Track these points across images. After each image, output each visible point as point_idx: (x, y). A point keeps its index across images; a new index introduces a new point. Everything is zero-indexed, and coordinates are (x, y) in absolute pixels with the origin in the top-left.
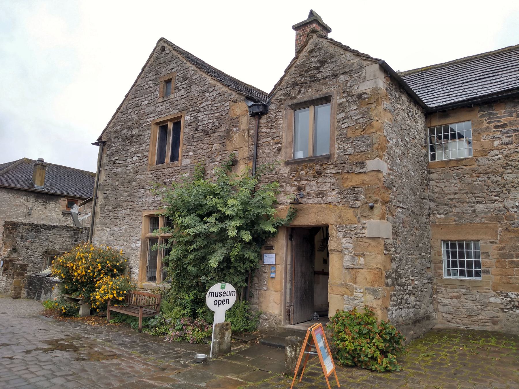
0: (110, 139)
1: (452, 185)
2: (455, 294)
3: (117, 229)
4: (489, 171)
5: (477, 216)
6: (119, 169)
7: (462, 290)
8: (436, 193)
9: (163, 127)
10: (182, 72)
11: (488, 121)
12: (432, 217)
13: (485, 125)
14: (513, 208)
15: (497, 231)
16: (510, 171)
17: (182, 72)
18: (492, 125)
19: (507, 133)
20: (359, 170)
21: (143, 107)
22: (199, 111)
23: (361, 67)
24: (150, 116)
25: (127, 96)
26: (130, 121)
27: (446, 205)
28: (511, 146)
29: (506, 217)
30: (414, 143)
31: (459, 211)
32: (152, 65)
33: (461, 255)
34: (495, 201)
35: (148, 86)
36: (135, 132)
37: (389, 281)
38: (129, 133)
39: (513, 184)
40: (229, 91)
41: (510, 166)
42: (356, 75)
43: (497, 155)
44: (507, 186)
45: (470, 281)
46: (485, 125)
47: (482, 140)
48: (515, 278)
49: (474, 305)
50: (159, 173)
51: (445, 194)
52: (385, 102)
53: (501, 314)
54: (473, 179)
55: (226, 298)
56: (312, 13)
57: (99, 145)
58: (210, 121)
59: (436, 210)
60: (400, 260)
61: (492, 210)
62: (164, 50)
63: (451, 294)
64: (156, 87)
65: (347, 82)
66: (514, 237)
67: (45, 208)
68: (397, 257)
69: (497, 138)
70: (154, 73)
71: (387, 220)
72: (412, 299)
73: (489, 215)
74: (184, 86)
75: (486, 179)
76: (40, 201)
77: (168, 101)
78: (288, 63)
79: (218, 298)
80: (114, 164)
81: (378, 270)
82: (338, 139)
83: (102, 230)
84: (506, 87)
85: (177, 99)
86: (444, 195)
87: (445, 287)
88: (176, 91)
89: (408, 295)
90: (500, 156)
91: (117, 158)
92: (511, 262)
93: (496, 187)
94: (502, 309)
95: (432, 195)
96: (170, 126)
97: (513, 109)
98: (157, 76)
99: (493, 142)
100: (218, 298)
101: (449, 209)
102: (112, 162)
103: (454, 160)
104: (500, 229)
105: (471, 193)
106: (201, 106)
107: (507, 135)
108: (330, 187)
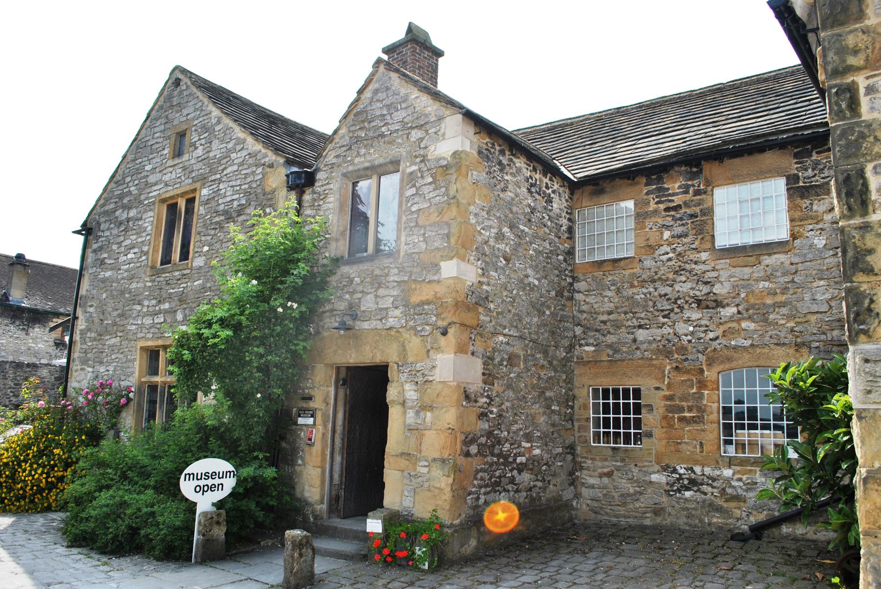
0: (99, 224)
1: (606, 299)
2: (606, 470)
3: (102, 369)
4: (656, 277)
5: (637, 349)
6: (108, 274)
7: (614, 463)
8: (584, 312)
9: (173, 208)
10: (201, 119)
11: (656, 200)
12: (577, 351)
13: (652, 206)
14: (686, 335)
15: (664, 371)
16: (683, 278)
17: (201, 119)
18: (662, 206)
19: (681, 219)
20: (430, 277)
21: (146, 173)
22: (220, 181)
23: (440, 119)
24: (155, 188)
25: (124, 157)
26: (127, 196)
27: (597, 330)
28: (685, 240)
29: (677, 349)
30: (541, 233)
31: (615, 340)
32: (161, 107)
33: (606, 410)
34: (664, 324)
35: (154, 142)
36: (133, 213)
37: (474, 449)
38: (125, 216)
39: (687, 299)
40: (263, 151)
41: (683, 270)
42: (434, 130)
43: (668, 253)
44: (679, 302)
45: (626, 450)
46: (652, 206)
47: (647, 230)
48: (685, 443)
49: (630, 485)
50: (162, 279)
51: (595, 313)
52: (475, 173)
53: (665, 499)
54: (635, 290)
55: (217, 481)
56: (411, 29)
57: (82, 234)
58: (234, 197)
59: (584, 339)
60: (500, 416)
61: (659, 338)
62: (181, 81)
63: (600, 471)
64: (166, 142)
65: (422, 139)
66: (686, 381)
67: (26, 334)
68: (492, 412)
69: (668, 227)
70: (163, 121)
71: (473, 354)
72: (526, 478)
73: (654, 345)
74: (203, 142)
75: (652, 290)
76: (18, 323)
77: (181, 165)
78: (344, 109)
79: (202, 483)
80: (101, 264)
81: (450, 431)
82: (405, 228)
83: (82, 369)
84: (682, 146)
85: (193, 161)
86: (595, 316)
87: (592, 459)
88: (191, 149)
89: (515, 472)
90: (671, 255)
91: (106, 255)
92: (681, 419)
93: (665, 303)
94: (667, 492)
95: (579, 315)
96: (182, 204)
97: (690, 183)
98: (167, 126)
99: (662, 234)
100: (202, 483)
101: (600, 337)
102: (99, 262)
103: (609, 260)
104: (668, 367)
105: (631, 312)
106: (225, 173)
107: (681, 223)
108: (393, 303)
